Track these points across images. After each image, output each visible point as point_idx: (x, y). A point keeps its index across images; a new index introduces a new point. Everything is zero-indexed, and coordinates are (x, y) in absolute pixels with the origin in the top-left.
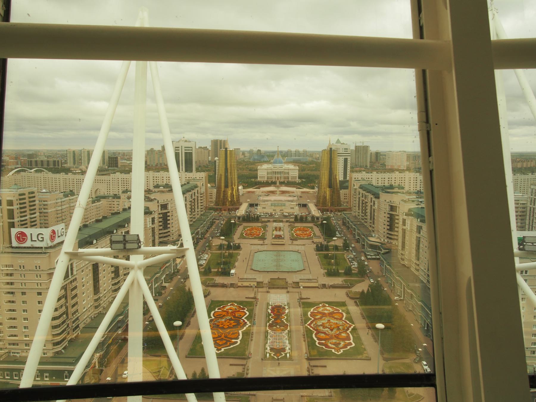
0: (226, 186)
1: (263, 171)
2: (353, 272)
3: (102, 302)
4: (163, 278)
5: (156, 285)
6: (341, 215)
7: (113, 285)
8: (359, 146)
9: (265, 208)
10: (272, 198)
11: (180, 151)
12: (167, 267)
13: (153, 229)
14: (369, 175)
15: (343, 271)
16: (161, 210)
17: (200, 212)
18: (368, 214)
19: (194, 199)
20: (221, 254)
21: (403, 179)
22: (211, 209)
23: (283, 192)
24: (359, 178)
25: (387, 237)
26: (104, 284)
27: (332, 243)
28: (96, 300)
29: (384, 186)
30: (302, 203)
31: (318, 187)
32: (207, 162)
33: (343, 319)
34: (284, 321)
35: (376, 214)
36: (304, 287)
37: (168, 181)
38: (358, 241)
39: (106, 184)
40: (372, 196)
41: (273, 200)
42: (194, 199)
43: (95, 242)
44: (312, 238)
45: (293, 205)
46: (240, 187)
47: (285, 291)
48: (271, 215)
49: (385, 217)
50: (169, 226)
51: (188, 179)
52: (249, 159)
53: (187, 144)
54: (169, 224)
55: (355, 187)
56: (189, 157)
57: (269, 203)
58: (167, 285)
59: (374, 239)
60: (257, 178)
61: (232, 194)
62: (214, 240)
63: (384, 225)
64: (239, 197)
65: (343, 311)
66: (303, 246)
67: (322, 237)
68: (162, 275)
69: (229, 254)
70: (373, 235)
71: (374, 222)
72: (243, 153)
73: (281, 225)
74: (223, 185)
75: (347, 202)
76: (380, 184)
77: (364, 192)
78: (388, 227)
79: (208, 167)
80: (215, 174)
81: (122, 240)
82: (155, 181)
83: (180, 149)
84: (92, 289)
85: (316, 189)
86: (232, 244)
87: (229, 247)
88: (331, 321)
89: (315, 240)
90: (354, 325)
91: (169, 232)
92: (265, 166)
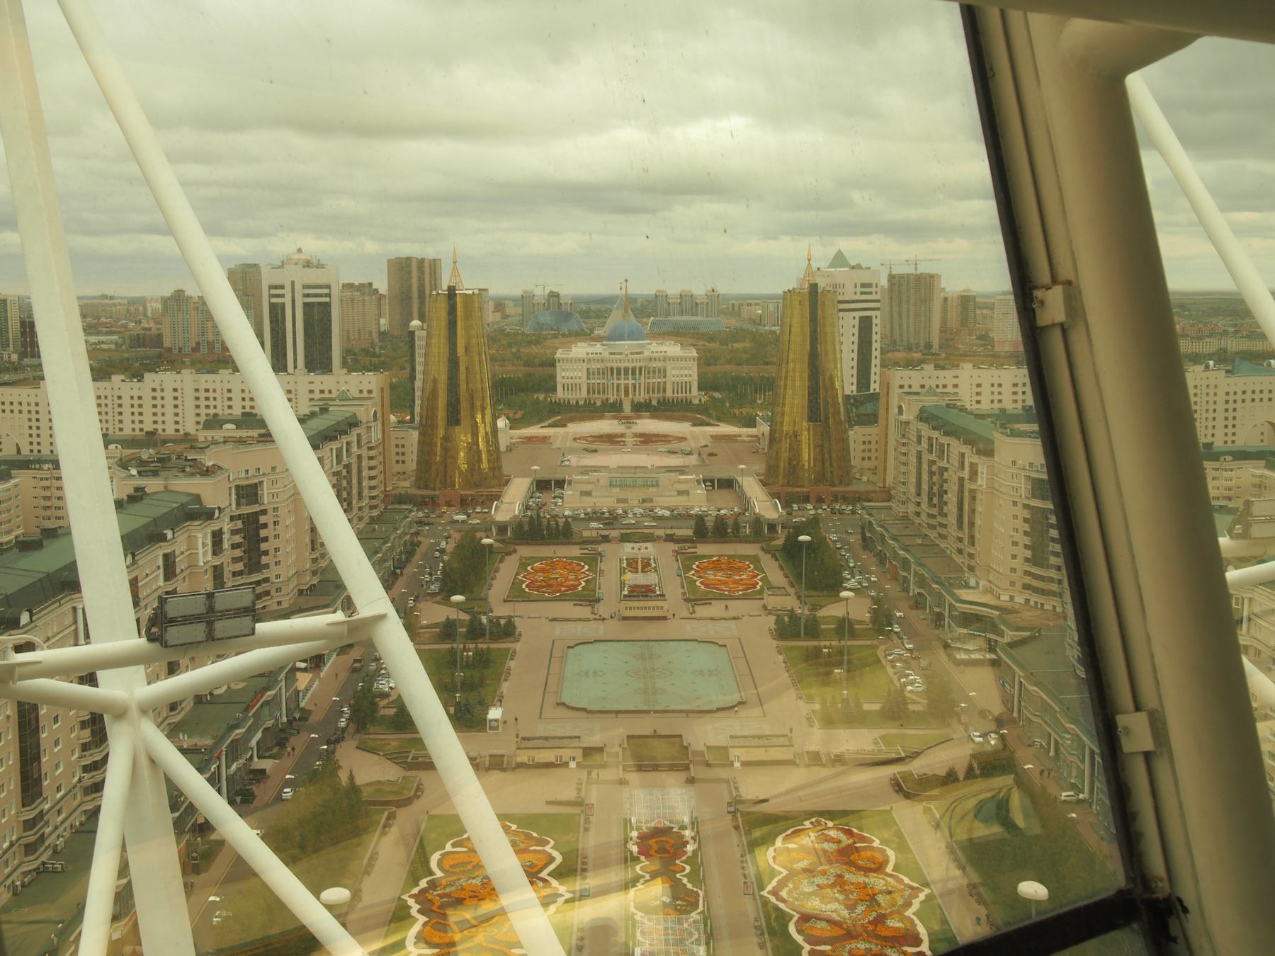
0: (454, 419)
1: (575, 364)
2: (911, 707)
3: (48, 830)
4: (253, 743)
5: (234, 767)
6: (853, 512)
7: (86, 769)
8: (901, 276)
9: (588, 494)
10: (613, 459)
11: (287, 300)
12: (267, 703)
14: (946, 376)
15: (877, 707)
16: (238, 504)
17: (367, 510)
18: (952, 508)
19: (348, 467)
20: (452, 652)
22: (401, 499)
23: (647, 440)
24: (907, 389)
26: (57, 766)
27: (833, 611)
28: (29, 825)
29: (1003, 410)
30: (718, 475)
31: (771, 421)
32: (375, 336)
33: (889, 869)
34: (685, 881)
35: (979, 509)
36: (744, 764)
37: (248, 403)
38: (918, 603)
39: (25, 415)
40: (965, 449)
41: (613, 466)
42: (348, 467)
43: (25, 618)
44: (759, 595)
45: (686, 481)
46: (502, 423)
47: (683, 776)
48: (611, 520)
49: (1015, 517)
51: (317, 395)
52: (522, 323)
53: (313, 276)
54: (266, 553)
55: (904, 417)
56: (318, 318)
57: (603, 477)
58: (266, 764)
59: (972, 596)
60: (554, 389)
61: (473, 450)
62: (423, 605)
63: (1015, 544)
64: (498, 459)
65: (883, 841)
66: (733, 624)
67: (791, 591)
68: (251, 732)
69: (479, 653)
70: (972, 582)
71: (972, 538)
72: (500, 305)
73: (649, 550)
74: (441, 414)
75: (874, 471)
76: (986, 406)
77: (935, 434)
78: (1029, 553)
79: (386, 354)
80: (413, 378)
81: (201, 609)
82: (203, 403)
83: (287, 292)
84: (14, 784)
85: (763, 428)
86: (484, 620)
87: (475, 631)
88: (847, 877)
89: (772, 601)
90: (927, 891)
91: (266, 580)
92: (581, 349)
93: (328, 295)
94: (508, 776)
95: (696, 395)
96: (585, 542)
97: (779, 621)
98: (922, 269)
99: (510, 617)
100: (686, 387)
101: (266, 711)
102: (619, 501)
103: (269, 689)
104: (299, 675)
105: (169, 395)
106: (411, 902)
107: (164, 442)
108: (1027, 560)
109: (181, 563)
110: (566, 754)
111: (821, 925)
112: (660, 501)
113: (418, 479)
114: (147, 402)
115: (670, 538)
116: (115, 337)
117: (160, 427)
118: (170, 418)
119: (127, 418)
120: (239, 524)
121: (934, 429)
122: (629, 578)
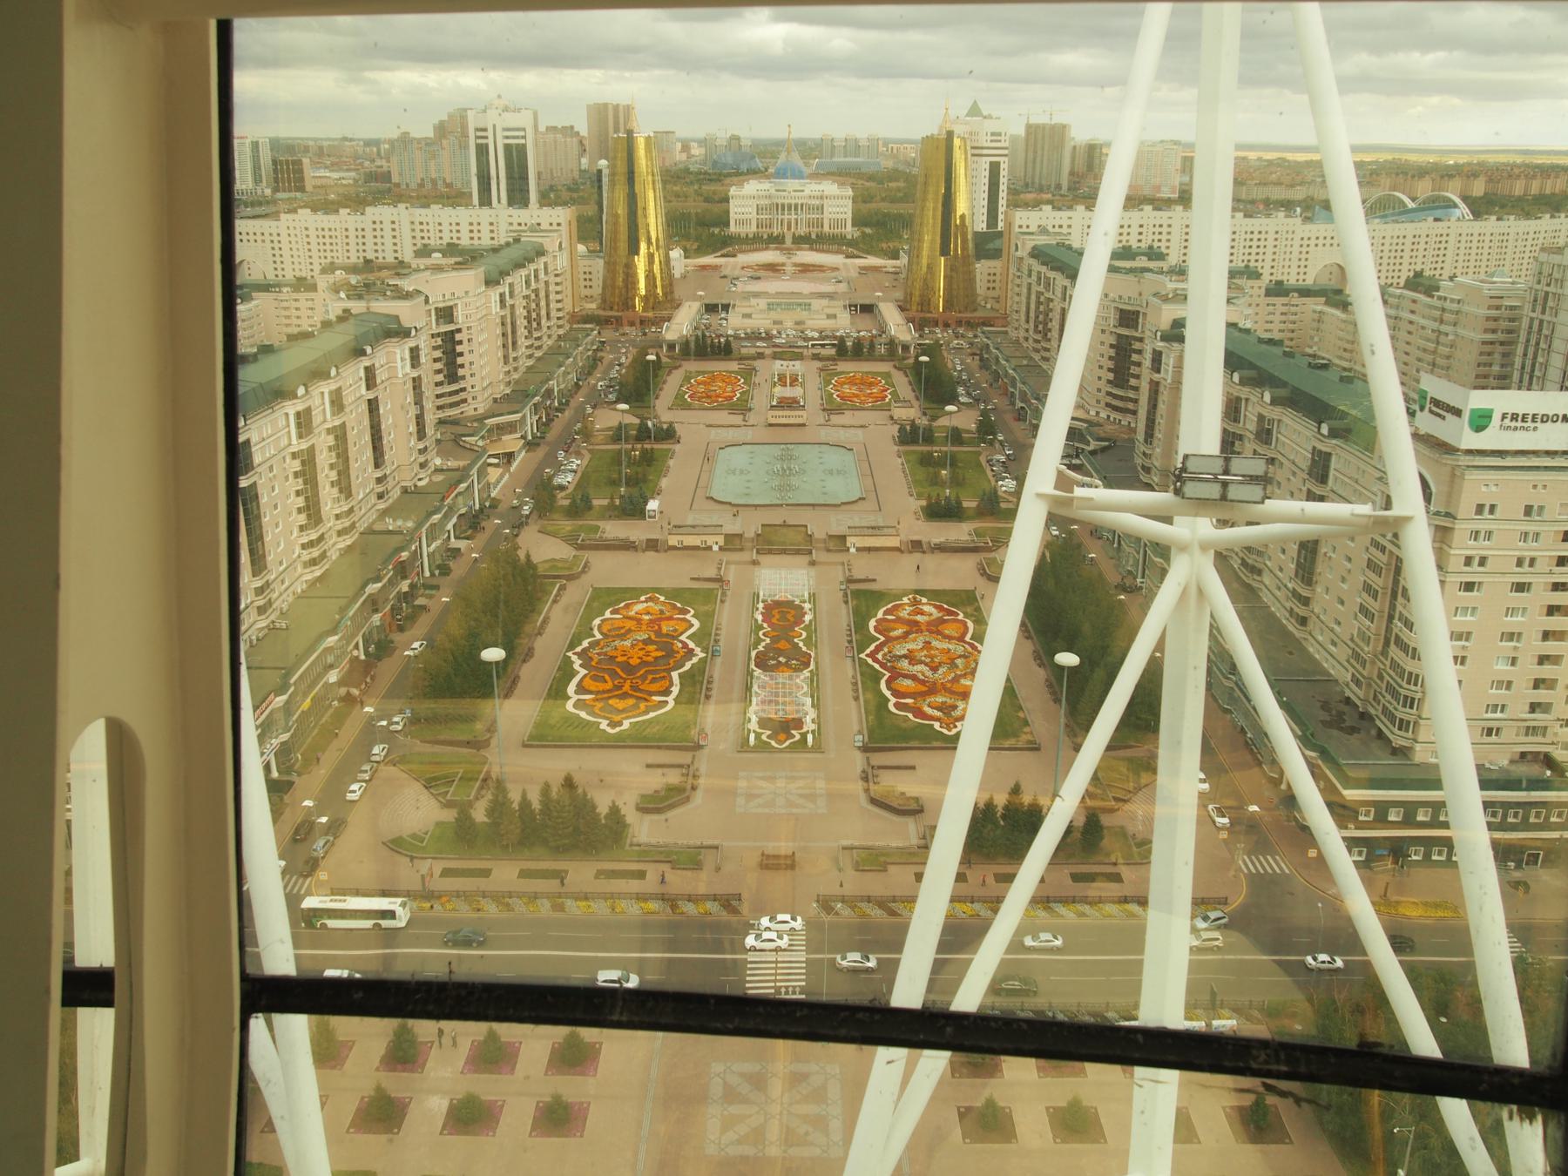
1: (746, 203)
2: (1003, 505)
3: (275, 596)
4: (450, 526)
8: (1037, 127)
9: (748, 316)
10: (772, 286)
13: (417, 383)
14: (1062, 217)
16: (437, 324)
19: (536, 291)
21: (1165, 230)
22: (588, 319)
23: (805, 269)
25: (1108, 405)
33: (967, 638)
36: (858, 549)
46: (676, 254)
50: (461, 372)
53: (512, 120)
55: (1019, 254)
56: (516, 158)
58: (462, 544)
60: (727, 224)
65: (966, 615)
66: (860, 432)
67: (916, 403)
68: (447, 517)
73: (797, 367)
75: (997, 300)
77: (1043, 269)
78: (1111, 376)
82: (419, 234)
83: (490, 134)
85: (904, 260)
92: (753, 187)
93: (524, 137)
94: (662, 555)
95: (850, 231)
96: (742, 359)
97: (902, 429)
98: (1058, 119)
99: (671, 424)
100: (843, 223)
101: (460, 499)
102: (775, 323)
103: (460, 482)
104: (490, 469)
105: (387, 226)
106: (574, 658)
107: (380, 268)
108: (1109, 382)
109: (381, 376)
110: (710, 540)
111: (908, 682)
112: (810, 323)
113: (604, 301)
114: (369, 234)
115: (816, 357)
116: (353, 174)
117: (380, 255)
118: (389, 247)
119: (353, 248)
120: (439, 341)
121: (1043, 264)
122: (779, 391)
